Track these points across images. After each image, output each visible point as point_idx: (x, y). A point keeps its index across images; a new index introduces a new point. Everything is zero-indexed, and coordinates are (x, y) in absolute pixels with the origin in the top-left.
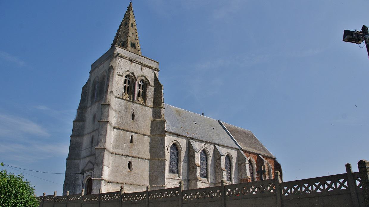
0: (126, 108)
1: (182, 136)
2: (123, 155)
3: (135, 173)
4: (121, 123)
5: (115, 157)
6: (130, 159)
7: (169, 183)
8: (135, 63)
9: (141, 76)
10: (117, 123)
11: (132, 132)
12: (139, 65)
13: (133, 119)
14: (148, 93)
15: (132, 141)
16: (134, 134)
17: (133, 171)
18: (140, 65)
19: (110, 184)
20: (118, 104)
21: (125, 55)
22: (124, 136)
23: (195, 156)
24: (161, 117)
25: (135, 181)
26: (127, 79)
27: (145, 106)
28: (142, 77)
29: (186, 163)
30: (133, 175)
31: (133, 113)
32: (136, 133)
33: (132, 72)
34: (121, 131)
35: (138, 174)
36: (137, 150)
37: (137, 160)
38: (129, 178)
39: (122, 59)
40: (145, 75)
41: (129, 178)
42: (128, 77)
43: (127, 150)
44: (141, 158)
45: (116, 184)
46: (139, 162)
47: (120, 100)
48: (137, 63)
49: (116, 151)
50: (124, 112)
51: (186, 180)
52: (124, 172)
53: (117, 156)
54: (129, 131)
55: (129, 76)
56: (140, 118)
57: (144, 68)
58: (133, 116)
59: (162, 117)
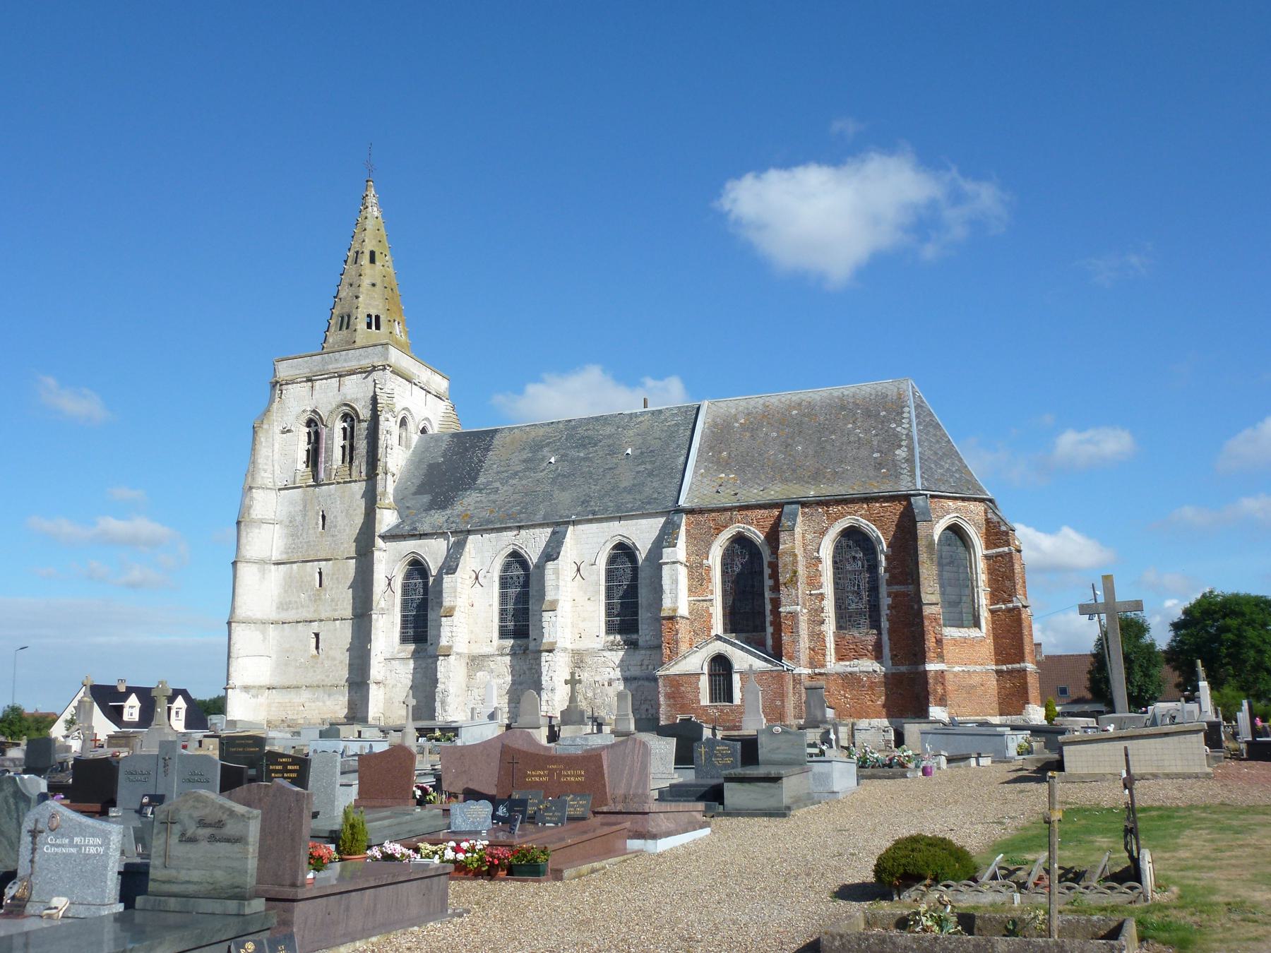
2: (297, 622)
4: (294, 548)
5: (264, 633)
6: (315, 627)
8: (321, 379)
9: (338, 407)
18: (335, 377)
21: (298, 372)
25: (328, 676)
28: (340, 409)
34: (295, 566)
35: (334, 659)
38: (315, 671)
45: (284, 690)
46: (335, 630)
49: (291, 615)
50: (299, 518)
56: (339, 519)
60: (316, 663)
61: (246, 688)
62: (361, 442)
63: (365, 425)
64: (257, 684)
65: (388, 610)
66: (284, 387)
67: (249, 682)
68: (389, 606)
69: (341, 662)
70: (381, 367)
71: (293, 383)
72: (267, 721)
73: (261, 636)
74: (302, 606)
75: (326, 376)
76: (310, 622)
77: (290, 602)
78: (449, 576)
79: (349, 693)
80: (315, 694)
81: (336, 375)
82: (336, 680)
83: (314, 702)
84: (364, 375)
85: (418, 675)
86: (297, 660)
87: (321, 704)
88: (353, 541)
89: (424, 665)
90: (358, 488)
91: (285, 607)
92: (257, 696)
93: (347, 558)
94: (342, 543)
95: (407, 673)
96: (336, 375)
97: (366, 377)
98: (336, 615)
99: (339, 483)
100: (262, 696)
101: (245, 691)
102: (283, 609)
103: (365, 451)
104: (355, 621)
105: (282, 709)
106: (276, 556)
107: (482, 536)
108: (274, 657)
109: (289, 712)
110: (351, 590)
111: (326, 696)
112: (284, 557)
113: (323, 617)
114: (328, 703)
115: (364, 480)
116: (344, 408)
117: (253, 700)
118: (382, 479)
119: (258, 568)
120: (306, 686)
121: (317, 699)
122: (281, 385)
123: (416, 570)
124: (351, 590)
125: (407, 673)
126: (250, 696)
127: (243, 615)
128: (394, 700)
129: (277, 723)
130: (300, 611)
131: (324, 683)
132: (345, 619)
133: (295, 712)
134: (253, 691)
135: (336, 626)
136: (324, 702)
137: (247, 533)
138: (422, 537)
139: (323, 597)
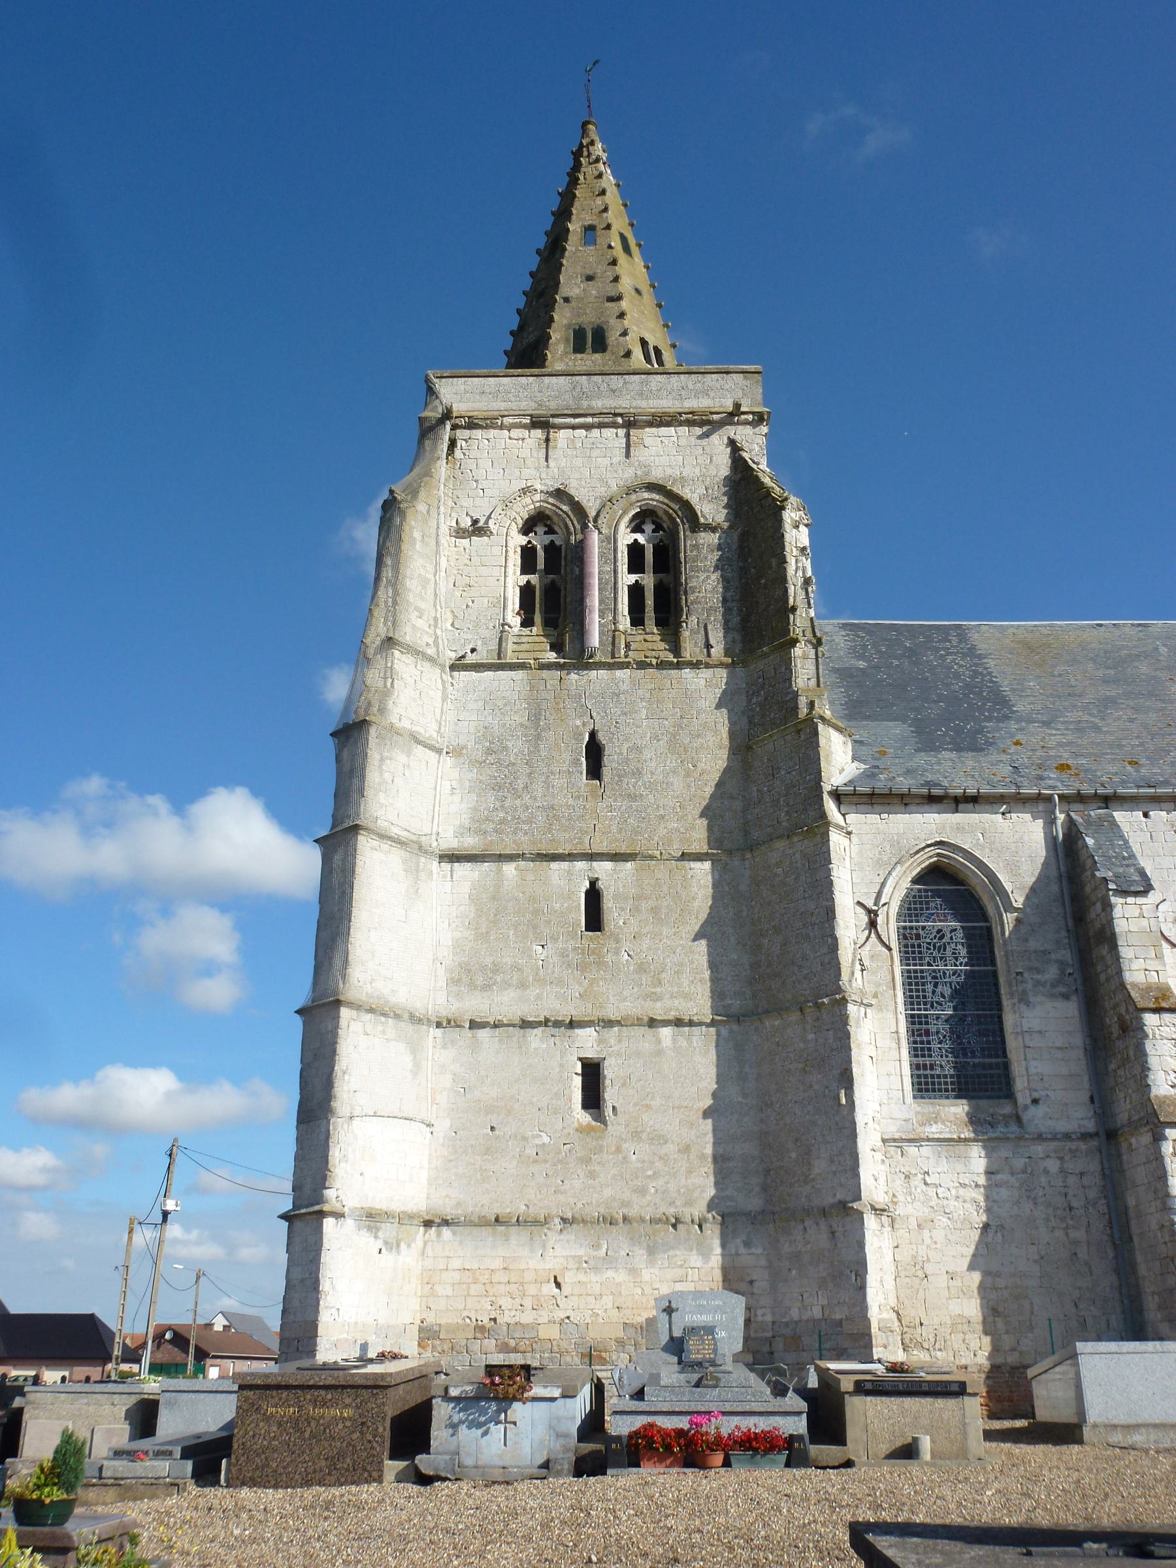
0: (536, 716)
1: (1000, 799)
2: (525, 1024)
3: (636, 1135)
4: (503, 821)
5: (415, 1049)
6: (587, 1042)
7: (917, 1181)
8: (574, 427)
9: (630, 490)
10: (477, 825)
11: (591, 857)
12: (609, 433)
13: (595, 770)
14: (693, 583)
15: (594, 920)
16: (603, 869)
17: (616, 1126)
18: (614, 425)
19: (446, 1232)
20: (472, 706)
21: (502, 406)
22: (533, 899)
23: (1120, 926)
24: (796, 708)
25: (642, 1191)
26: (539, 541)
27: (678, 666)
28: (634, 497)
29: (1066, 997)
30: (618, 1150)
31: (593, 735)
32: (616, 857)
33: (554, 485)
34: (509, 869)
35: (659, 1139)
36: (642, 968)
37: (642, 1039)
38: (592, 1175)
39: (478, 433)
40: (657, 475)
41: (592, 1175)
42: (540, 529)
43: (560, 982)
44: (678, 1023)
45: (486, 1231)
46: (660, 1053)
47: (489, 674)
48: (588, 427)
49: (476, 1005)
50: (517, 746)
51: (1085, 1136)
52: (546, 1139)
53: (483, 1034)
54: (570, 857)
55: (548, 518)
56: (647, 754)
57: (649, 435)
58: (595, 753)
59: (803, 701)
60: (599, 1150)
61: (372, 1218)
62: (702, 576)
63: (713, 538)
64: (396, 1207)
65: (875, 996)
66: (460, 433)
67: (380, 1202)
68: (878, 985)
69: (686, 1149)
70: (750, 417)
71: (487, 427)
72: (421, 1330)
73: (408, 1060)
74: (541, 982)
75: (589, 420)
76: (572, 1025)
77: (496, 969)
78: (1130, 900)
79: (723, 1246)
80: (597, 1246)
81: (620, 420)
82: (672, 1203)
83: (596, 1269)
84: (698, 431)
85: (1004, 1193)
86: (524, 1139)
87: (621, 1276)
88: (697, 812)
89: (1019, 1163)
90: (703, 682)
91: (480, 980)
92: (398, 1245)
93: (684, 857)
94: (662, 817)
95: (963, 1185)
96: (620, 420)
97: (706, 435)
98: (658, 1010)
99: (642, 665)
100: (409, 1246)
101: (369, 1228)
102: (472, 986)
103: (716, 600)
104: (724, 1031)
105: (475, 1289)
106: (450, 842)
107: (1146, 815)
108: (443, 1126)
109: (505, 1302)
110: (703, 942)
111: (640, 1254)
112: (471, 843)
113: (612, 1013)
114: (647, 1275)
115: (721, 665)
116: (646, 495)
117: (387, 1258)
118: (805, 657)
119: (405, 862)
120: (564, 1220)
121: (609, 1260)
122: (455, 427)
123: (936, 893)
124: (703, 942)
125: (963, 1185)
126: (379, 1244)
127: (368, 988)
128: (929, 1268)
129: (460, 1339)
130: (533, 992)
131: (632, 1212)
132: (691, 1023)
133: (528, 1302)
134: (388, 1230)
135: (659, 1042)
136: (633, 1271)
137: (382, 760)
138: (961, 806)
139: (609, 958)
